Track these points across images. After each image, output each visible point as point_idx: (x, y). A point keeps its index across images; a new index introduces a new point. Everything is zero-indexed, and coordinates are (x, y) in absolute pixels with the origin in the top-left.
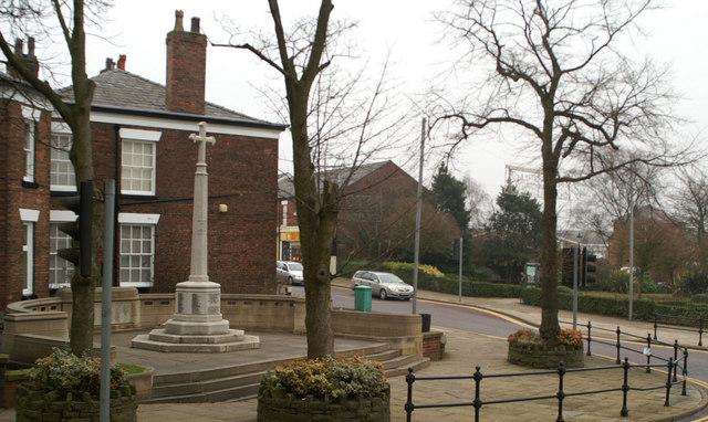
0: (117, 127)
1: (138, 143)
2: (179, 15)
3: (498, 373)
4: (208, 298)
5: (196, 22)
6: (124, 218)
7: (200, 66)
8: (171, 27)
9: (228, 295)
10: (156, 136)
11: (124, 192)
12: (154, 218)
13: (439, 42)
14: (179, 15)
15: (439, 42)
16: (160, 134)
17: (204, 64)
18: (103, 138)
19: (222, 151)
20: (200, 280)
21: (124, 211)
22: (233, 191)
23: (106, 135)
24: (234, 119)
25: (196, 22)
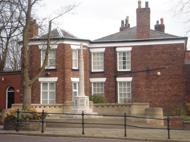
0: (115, 48)
1: (98, 53)
2: (139, 3)
3: (76, 124)
4: (79, 101)
5: (147, 3)
6: (119, 79)
7: (148, 20)
8: (137, 7)
9: (95, 104)
10: (103, 50)
11: (93, 71)
12: (130, 79)
13: (44, 19)
14: (139, 3)
15: (44, 19)
16: (105, 49)
17: (149, 19)
18: (111, 52)
19: (158, 51)
20: (83, 95)
21: (118, 77)
22: (164, 67)
23: (111, 51)
24: (171, 38)
25: (147, 3)
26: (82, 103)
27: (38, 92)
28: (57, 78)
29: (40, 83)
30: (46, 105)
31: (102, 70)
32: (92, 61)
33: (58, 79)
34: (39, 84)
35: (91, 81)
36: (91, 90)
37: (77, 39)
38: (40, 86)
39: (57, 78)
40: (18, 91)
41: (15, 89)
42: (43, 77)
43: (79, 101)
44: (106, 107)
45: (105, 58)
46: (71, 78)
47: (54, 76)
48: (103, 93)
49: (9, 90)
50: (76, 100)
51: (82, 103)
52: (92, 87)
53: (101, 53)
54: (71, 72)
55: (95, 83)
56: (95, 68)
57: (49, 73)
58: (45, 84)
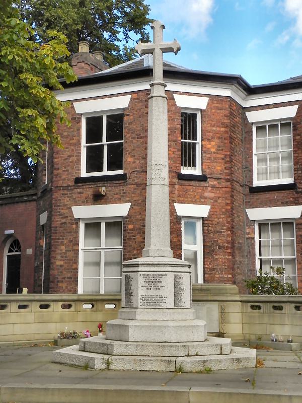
1: (273, 126)
11: (257, 183)
26: (152, 292)
27: (71, 254)
28: (128, 205)
29: (77, 224)
30: (75, 297)
31: (289, 181)
32: (255, 151)
33: (131, 207)
34: (74, 226)
35: (251, 218)
36: (254, 248)
37: (176, 70)
38: (77, 232)
39: (128, 205)
40: (29, 251)
41: (22, 248)
42: (85, 202)
43: (141, 281)
44: (294, 310)
45: (298, 137)
46: (209, 207)
47: (120, 200)
48: (295, 257)
49: (10, 251)
50: (128, 278)
51: (152, 292)
52: (253, 238)
53: (286, 124)
54: (177, 187)
55: (263, 225)
56: (263, 174)
57: (103, 190)
58: (93, 226)
